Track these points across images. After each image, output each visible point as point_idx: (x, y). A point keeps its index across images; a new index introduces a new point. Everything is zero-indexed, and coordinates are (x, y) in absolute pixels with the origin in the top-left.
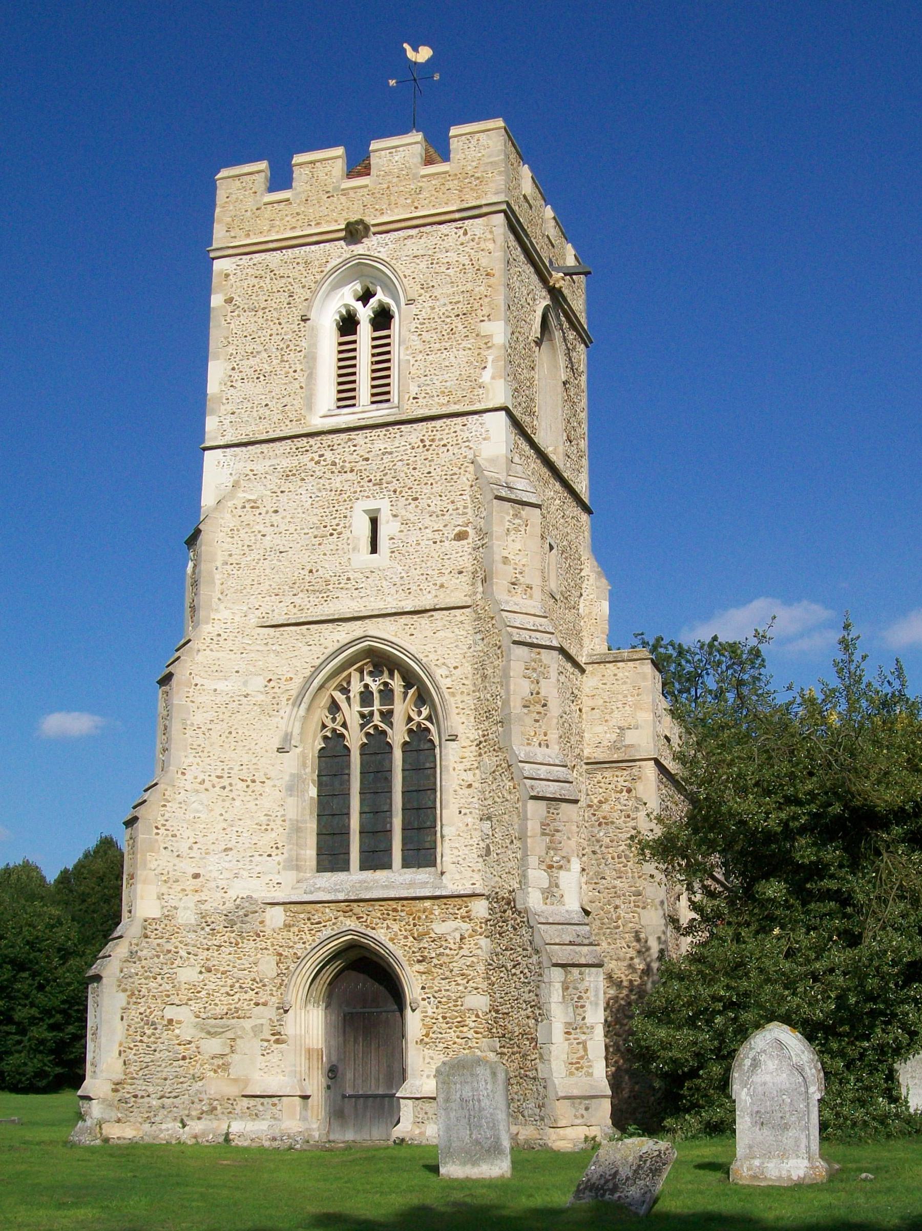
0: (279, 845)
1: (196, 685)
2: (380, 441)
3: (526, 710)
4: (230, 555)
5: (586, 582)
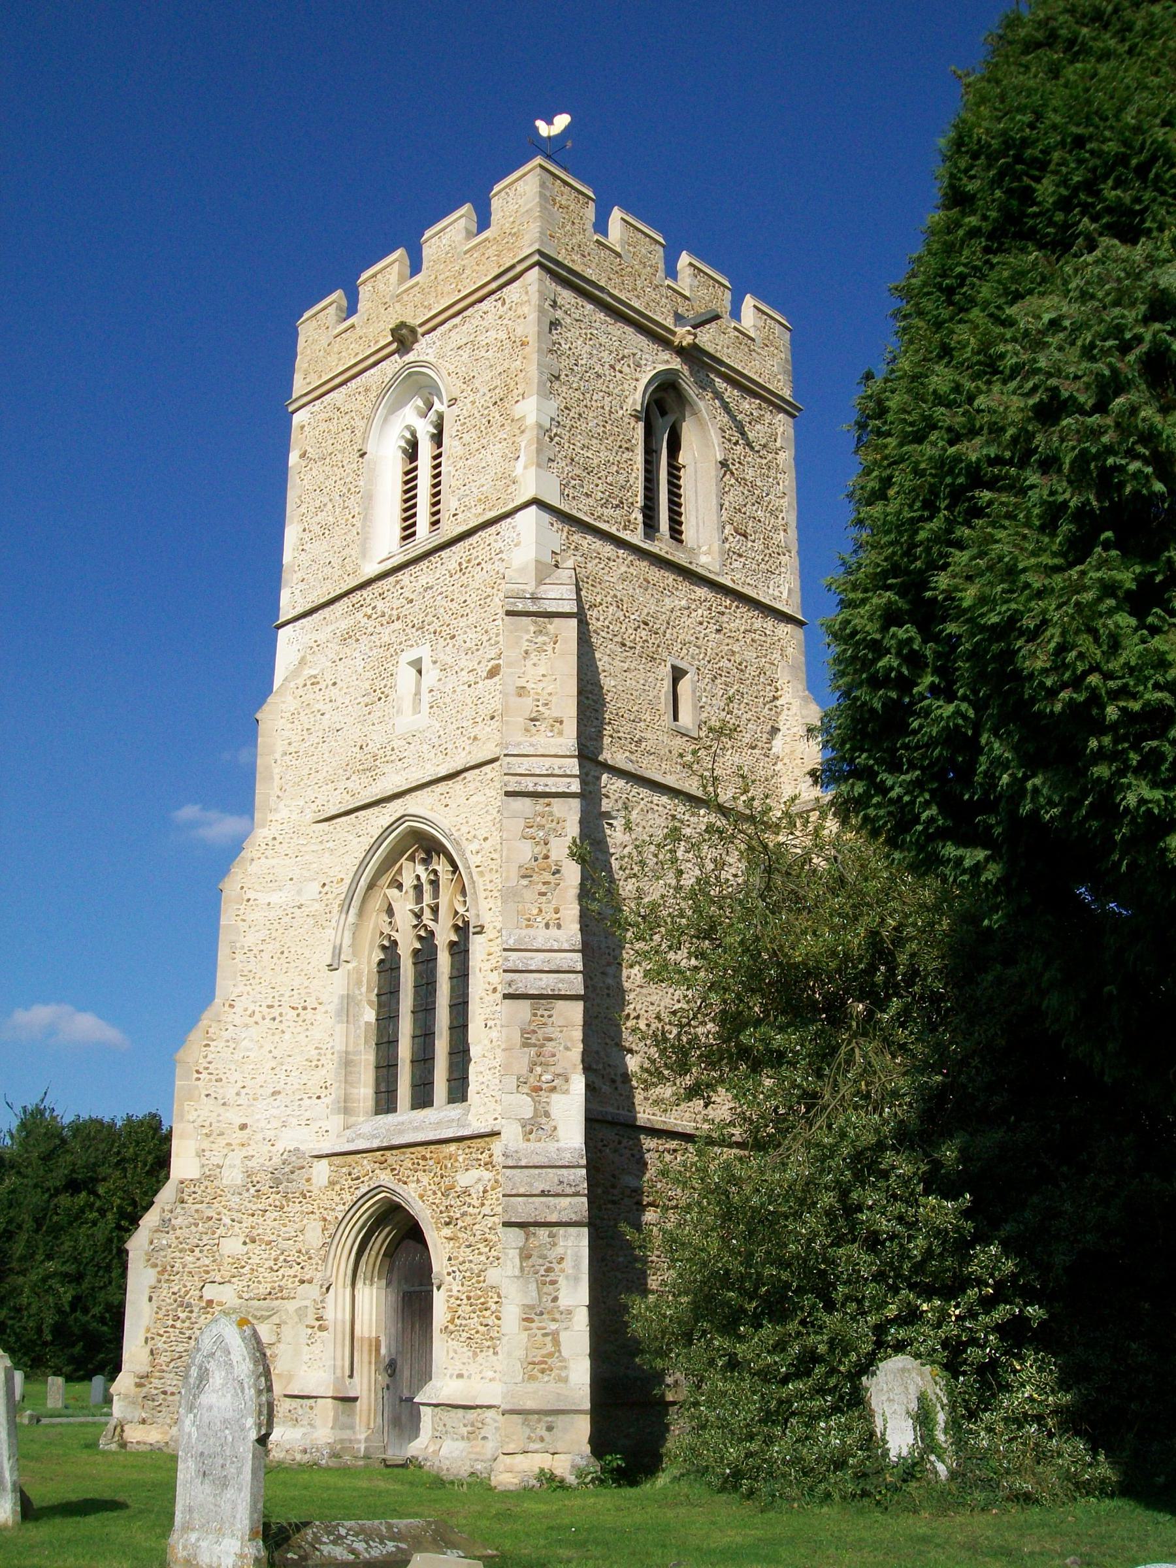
1: (249, 900)
3: (525, 882)
4: (290, 744)
5: (785, 712)
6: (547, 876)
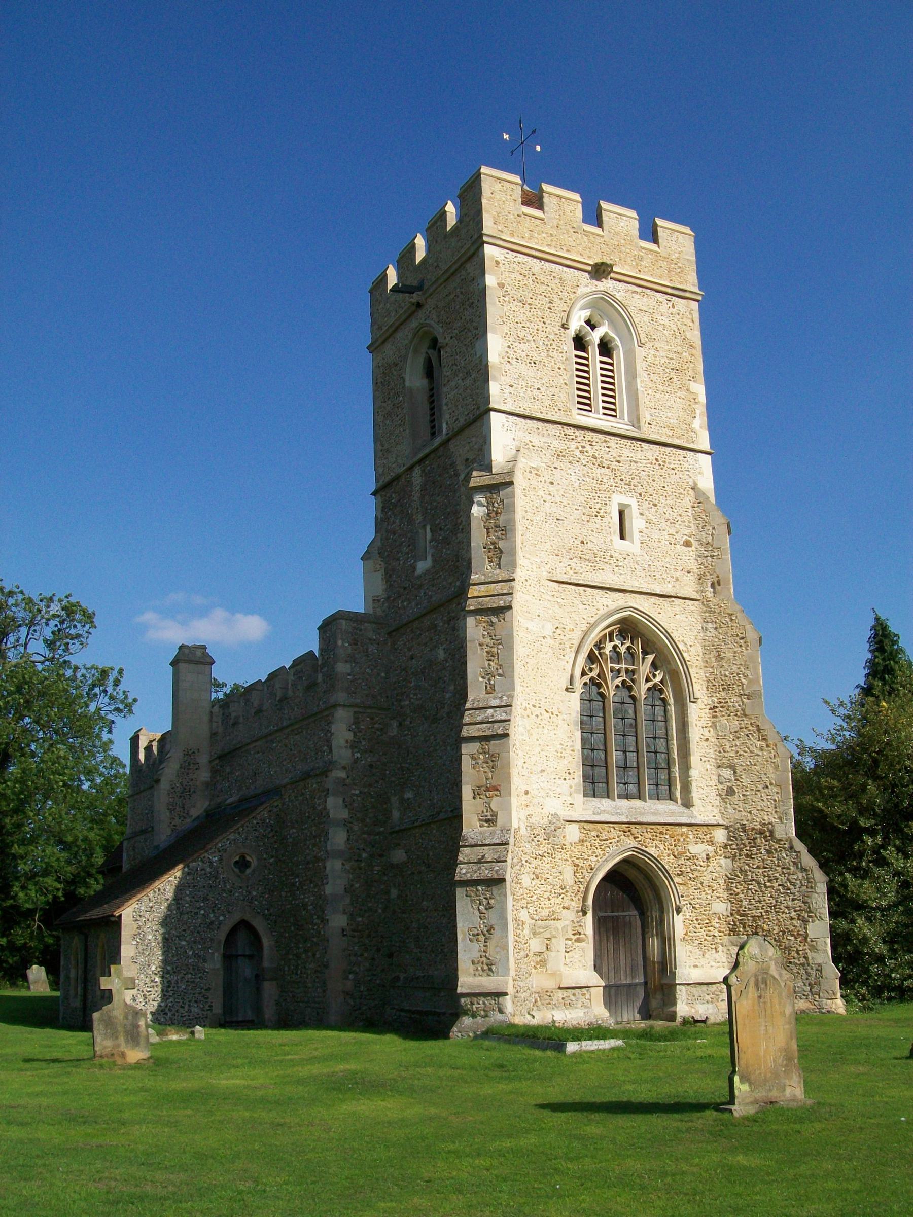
0: (571, 771)
2: (627, 450)
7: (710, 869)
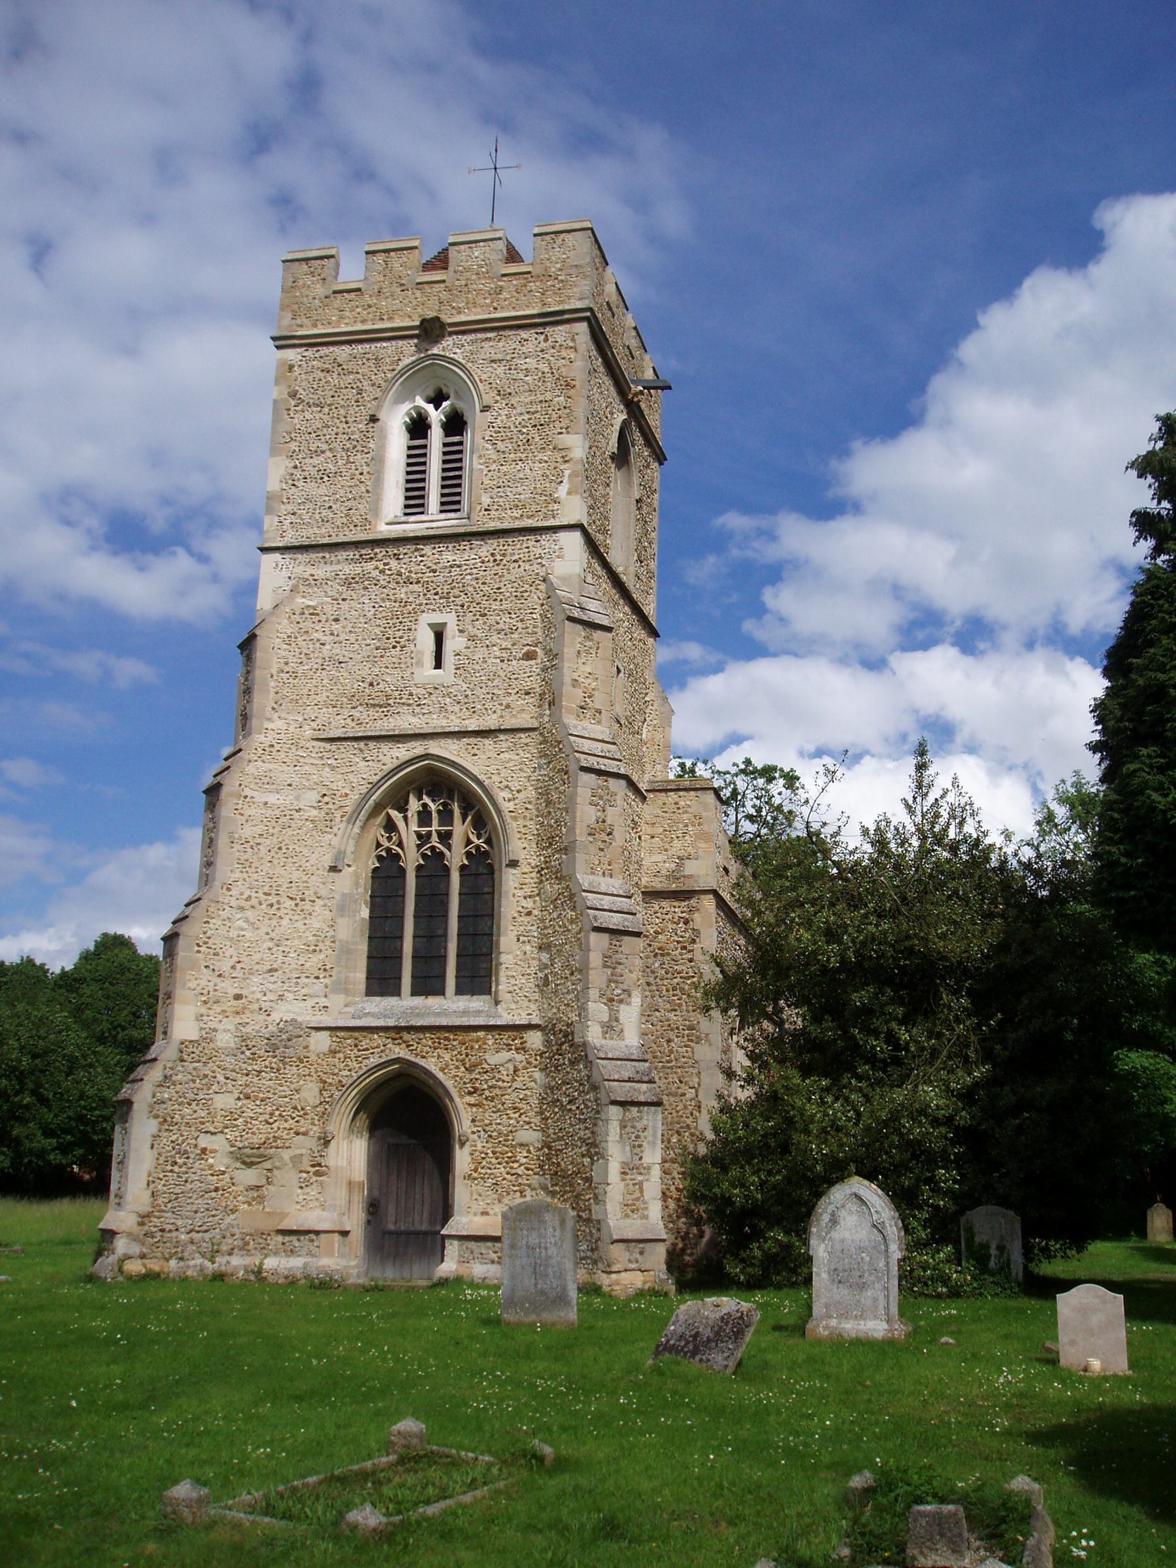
1: (246, 797)
4: (286, 664)
6: (604, 837)
7: (515, 1085)
